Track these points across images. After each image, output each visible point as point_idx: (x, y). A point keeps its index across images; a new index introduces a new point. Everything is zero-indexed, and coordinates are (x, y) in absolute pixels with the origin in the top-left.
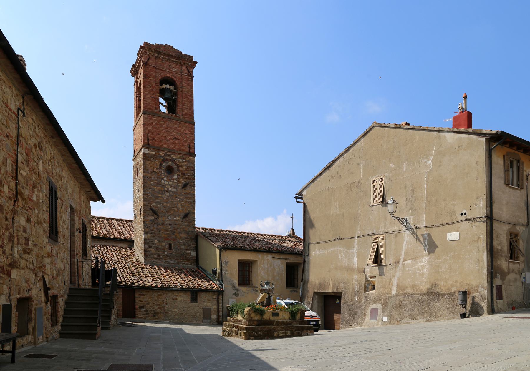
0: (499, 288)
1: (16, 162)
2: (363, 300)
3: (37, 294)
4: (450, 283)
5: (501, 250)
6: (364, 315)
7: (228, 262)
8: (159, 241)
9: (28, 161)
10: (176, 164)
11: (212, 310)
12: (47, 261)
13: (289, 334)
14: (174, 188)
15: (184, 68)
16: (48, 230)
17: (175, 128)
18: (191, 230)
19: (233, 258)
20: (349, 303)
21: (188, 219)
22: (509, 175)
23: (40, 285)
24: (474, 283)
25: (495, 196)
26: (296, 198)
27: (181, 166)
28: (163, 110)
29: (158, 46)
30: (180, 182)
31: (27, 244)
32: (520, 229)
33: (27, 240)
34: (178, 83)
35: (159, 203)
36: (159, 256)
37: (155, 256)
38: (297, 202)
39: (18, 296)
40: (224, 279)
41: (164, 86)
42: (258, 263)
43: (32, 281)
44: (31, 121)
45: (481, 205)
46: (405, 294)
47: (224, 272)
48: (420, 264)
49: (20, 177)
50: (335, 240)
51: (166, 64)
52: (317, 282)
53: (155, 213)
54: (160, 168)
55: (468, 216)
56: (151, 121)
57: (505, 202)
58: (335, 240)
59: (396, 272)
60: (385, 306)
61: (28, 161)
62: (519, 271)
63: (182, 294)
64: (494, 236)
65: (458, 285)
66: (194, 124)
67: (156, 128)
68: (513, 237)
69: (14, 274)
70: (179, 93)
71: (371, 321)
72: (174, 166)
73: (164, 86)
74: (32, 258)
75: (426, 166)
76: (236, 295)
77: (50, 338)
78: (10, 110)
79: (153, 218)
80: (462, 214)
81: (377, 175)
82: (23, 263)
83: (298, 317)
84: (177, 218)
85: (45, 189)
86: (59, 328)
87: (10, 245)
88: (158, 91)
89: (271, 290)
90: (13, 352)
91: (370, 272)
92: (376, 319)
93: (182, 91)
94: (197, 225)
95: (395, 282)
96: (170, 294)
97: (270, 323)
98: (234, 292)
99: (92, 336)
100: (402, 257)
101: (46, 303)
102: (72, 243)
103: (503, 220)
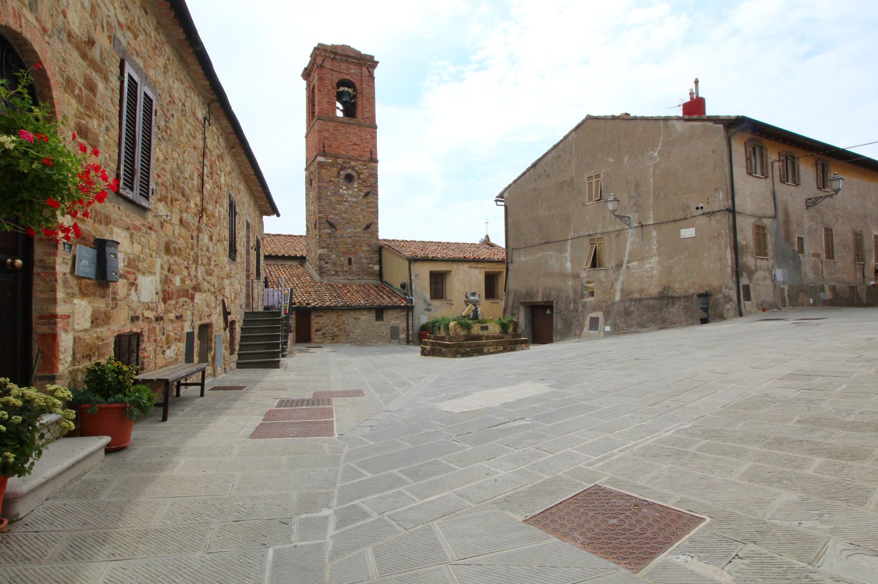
0: (747, 288)
1: (202, 176)
2: (580, 308)
3: (217, 320)
4: (686, 284)
5: (746, 246)
6: (581, 326)
8: (337, 256)
9: (212, 173)
10: (356, 171)
12: (227, 282)
13: (501, 349)
15: (364, 69)
16: (228, 249)
18: (374, 241)
19: (423, 272)
22: (751, 163)
23: (220, 309)
24: (716, 283)
25: (736, 187)
26: (496, 201)
28: (340, 114)
29: (333, 47)
30: (360, 190)
31: (209, 264)
32: (767, 222)
33: (209, 259)
34: (357, 85)
35: (337, 215)
36: (337, 272)
37: (333, 273)
39: (200, 323)
41: (341, 89)
42: (453, 273)
43: (213, 305)
44: (215, 130)
45: (721, 197)
46: (631, 300)
47: (413, 286)
48: (648, 266)
49: (205, 192)
51: (343, 66)
52: (524, 291)
53: (331, 225)
54: (338, 177)
55: (705, 210)
56: (327, 127)
57: (748, 193)
59: (619, 275)
60: (607, 315)
61: (212, 173)
62: (768, 268)
63: (365, 312)
64: (738, 230)
65: (696, 286)
66: (376, 128)
68: (760, 231)
69: (198, 296)
70: (359, 96)
71: (592, 332)
72: (354, 174)
73: (341, 89)
74: (214, 280)
75: (652, 158)
76: (428, 310)
77: (228, 368)
78: (197, 119)
79: (330, 231)
80: (697, 208)
82: (205, 286)
83: (511, 330)
84: (359, 230)
85: (226, 203)
86: (235, 357)
87: (194, 266)
89: (477, 301)
90: (202, 385)
91: (588, 277)
93: (362, 93)
94: (380, 238)
95: (618, 286)
96: (352, 313)
97: (479, 338)
98: (425, 307)
99: (276, 365)
100: (626, 259)
101: (225, 330)
102: (248, 261)
103: (747, 212)
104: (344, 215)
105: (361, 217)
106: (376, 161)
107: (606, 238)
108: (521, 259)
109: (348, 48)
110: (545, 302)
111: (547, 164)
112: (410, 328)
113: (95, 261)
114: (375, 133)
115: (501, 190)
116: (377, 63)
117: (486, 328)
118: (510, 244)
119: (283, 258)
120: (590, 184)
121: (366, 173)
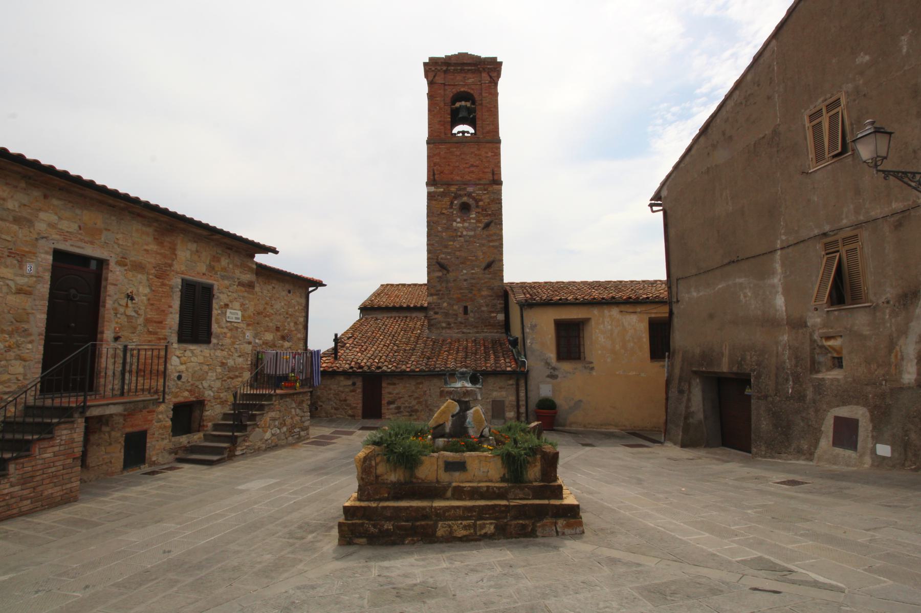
2: (810, 394)
6: (815, 435)
7: (536, 326)
8: (449, 304)
10: (474, 198)
11: (507, 403)
13: (490, 529)
14: (471, 230)
15: (484, 75)
17: (472, 153)
20: (770, 399)
21: (492, 270)
26: (651, 205)
27: (481, 200)
30: (479, 221)
35: (449, 254)
36: (449, 324)
37: (444, 325)
38: (653, 212)
40: (528, 353)
41: (458, 105)
42: (593, 322)
47: (528, 342)
50: (729, 263)
51: (459, 77)
52: (698, 351)
54: (451, 208)
58: (729, 263)
67: (444, 158)
71: (839, 451)
72: (471, 202)
73: (458, 105)
76: (553, 377)
79: (440, 274)
81: (820, 100)
83: (533, 473)
84: (477, 270)
88: (449, 111)
91: (825, 326)
92: (853, 446)
93: (481, 104)
96: (435, 381)
98: (548, 372)
104: (458, 253)
105: (480, 254)
106: (500, 183)
107: (865, 235)
108: (692, 295)
109: (466, 54)
110: (736, 374)
111: (726, 121)
112: (522, 403)
113: (100, 321)
114: (499, 148)
115: (657, 185)
116: (501, 63)
117: (460, 466)
118: (673, 271)
119: (408, 309)
120: (817, 129)
121: (486, 199)
